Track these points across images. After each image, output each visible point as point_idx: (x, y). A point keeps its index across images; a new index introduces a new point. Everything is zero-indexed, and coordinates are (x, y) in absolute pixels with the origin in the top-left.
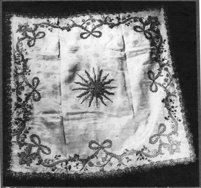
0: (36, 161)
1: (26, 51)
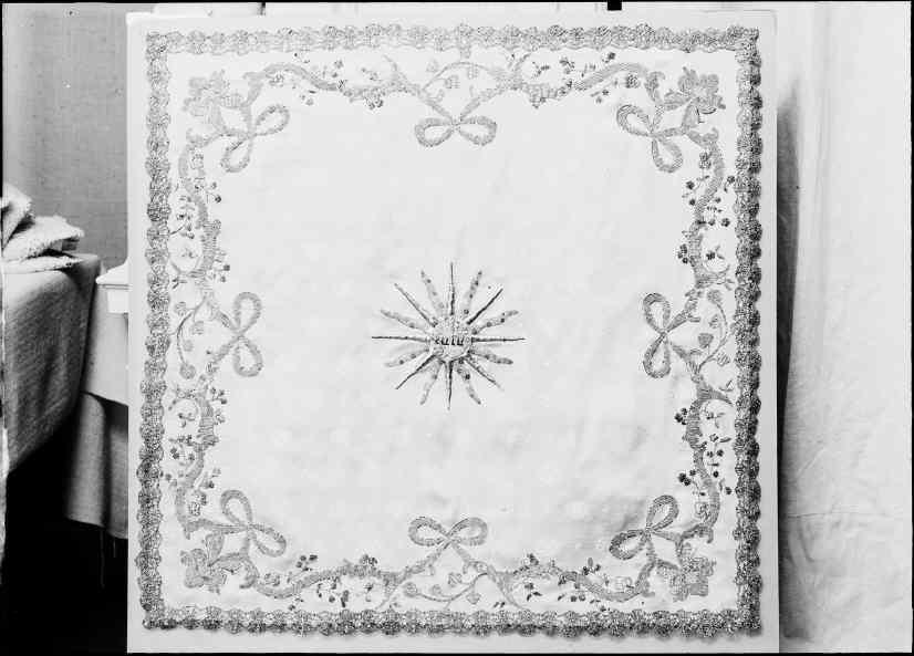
0: (240, 578)
1: (216, 192)
